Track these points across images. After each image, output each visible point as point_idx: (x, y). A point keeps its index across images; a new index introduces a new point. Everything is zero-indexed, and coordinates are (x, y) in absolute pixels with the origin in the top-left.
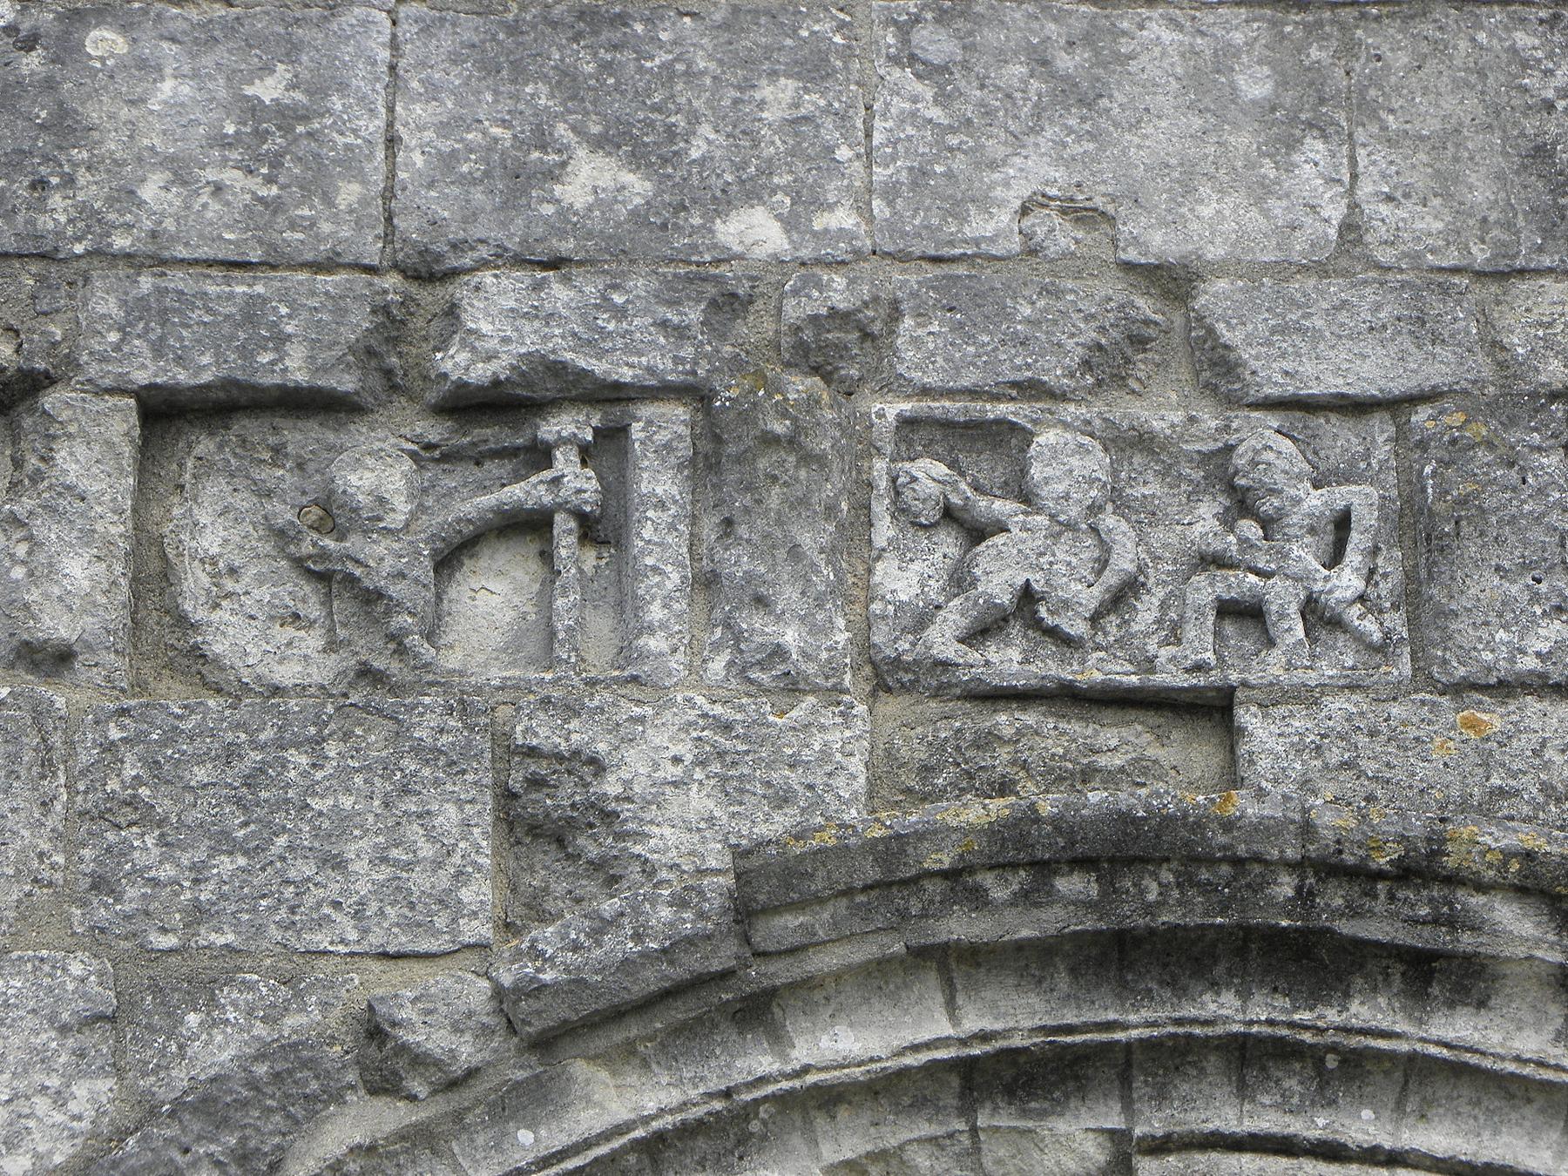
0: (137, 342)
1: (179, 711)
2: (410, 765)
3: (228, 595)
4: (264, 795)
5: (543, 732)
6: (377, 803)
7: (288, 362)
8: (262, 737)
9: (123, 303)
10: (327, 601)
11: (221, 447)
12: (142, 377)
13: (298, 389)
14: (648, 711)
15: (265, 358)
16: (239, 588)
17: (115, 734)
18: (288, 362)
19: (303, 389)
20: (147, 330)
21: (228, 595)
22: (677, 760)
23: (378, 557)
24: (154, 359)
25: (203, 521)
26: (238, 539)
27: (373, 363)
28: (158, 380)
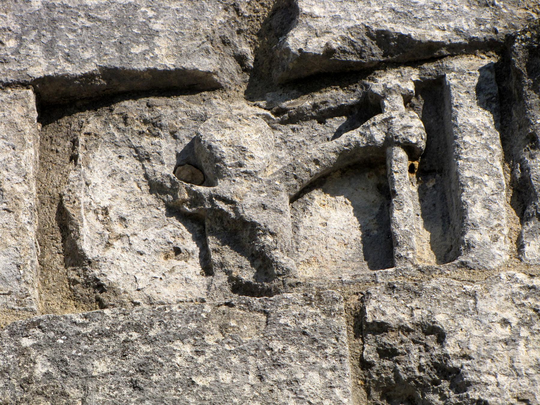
0: (32, 46)
1: (81, 321)
2: (277, 345)
3: (120, 237)
4: (155, 378)
5: (389, 311)
6: (251, 376)
7: (156, 51)
8: (152, 334)
9: (18, 18)
10: (201, 240)
11: (106, 123)
12: (39, 70)
13: (167, 73)
14: (478, 287)
15: (137, 50)
16: (128, 232)
17: (26, 342)
18: (156, 51)
19: (170, 72)
20: (40, 36)
21: (120, 237)
22: (505, 322)
23: (243, 195)
24: (46, 57)
25: (93, 181)
26: (124, 194)
27: (229, 50)
28: (51, 73)
